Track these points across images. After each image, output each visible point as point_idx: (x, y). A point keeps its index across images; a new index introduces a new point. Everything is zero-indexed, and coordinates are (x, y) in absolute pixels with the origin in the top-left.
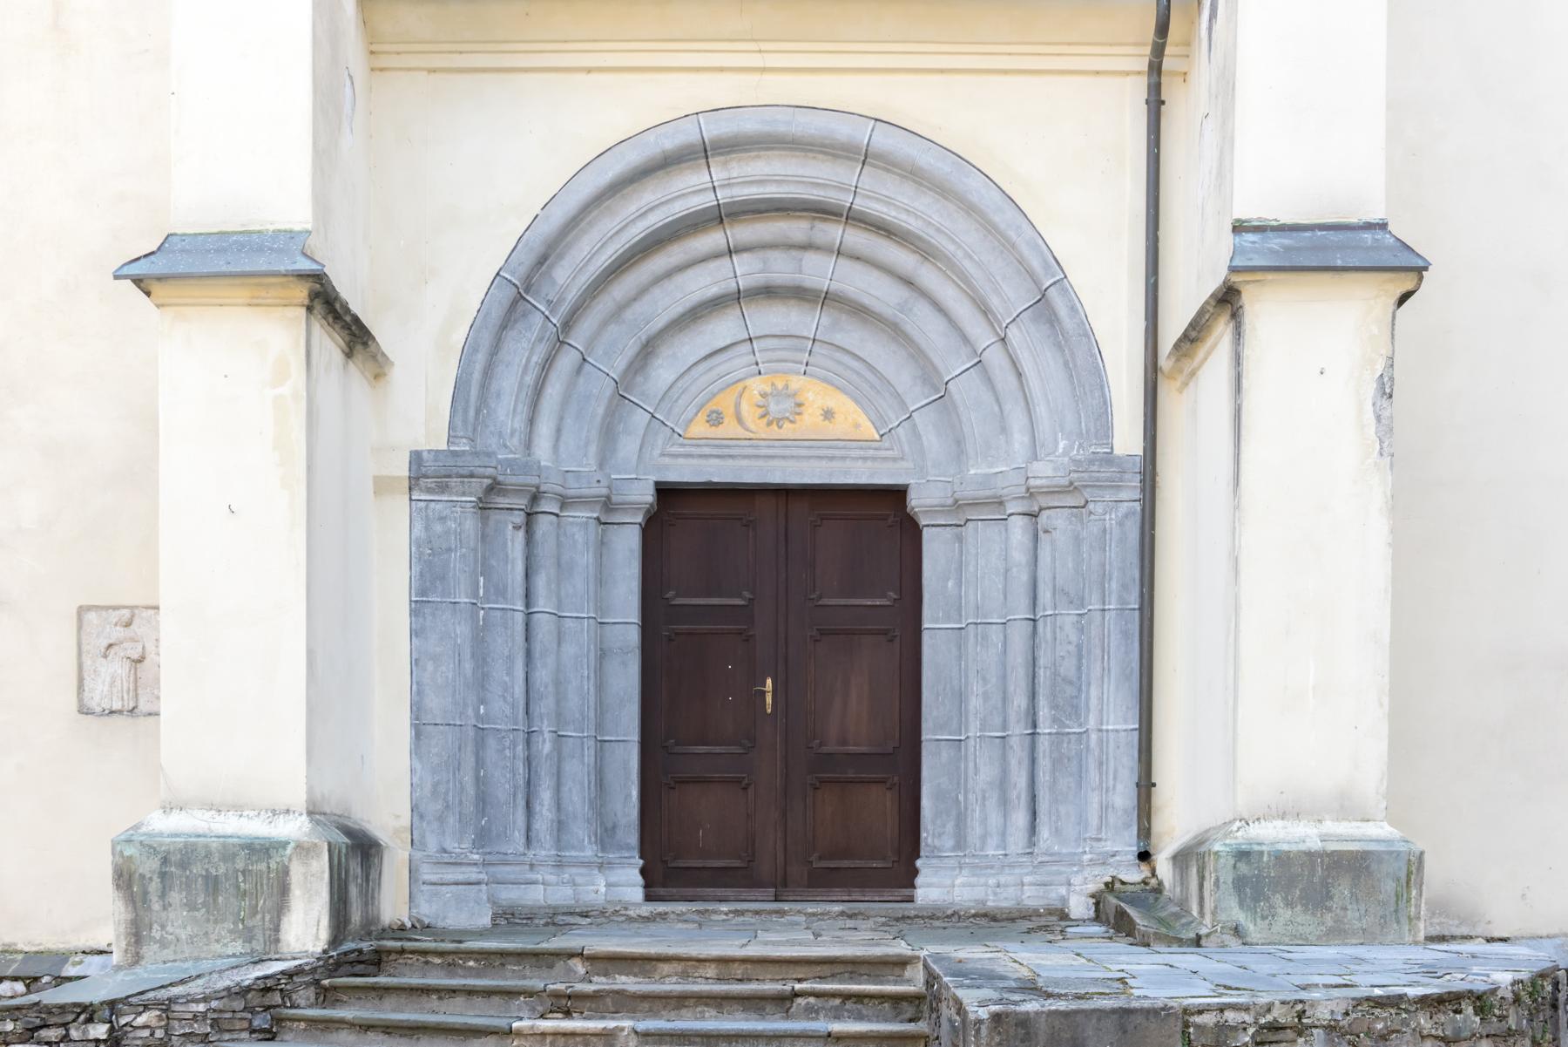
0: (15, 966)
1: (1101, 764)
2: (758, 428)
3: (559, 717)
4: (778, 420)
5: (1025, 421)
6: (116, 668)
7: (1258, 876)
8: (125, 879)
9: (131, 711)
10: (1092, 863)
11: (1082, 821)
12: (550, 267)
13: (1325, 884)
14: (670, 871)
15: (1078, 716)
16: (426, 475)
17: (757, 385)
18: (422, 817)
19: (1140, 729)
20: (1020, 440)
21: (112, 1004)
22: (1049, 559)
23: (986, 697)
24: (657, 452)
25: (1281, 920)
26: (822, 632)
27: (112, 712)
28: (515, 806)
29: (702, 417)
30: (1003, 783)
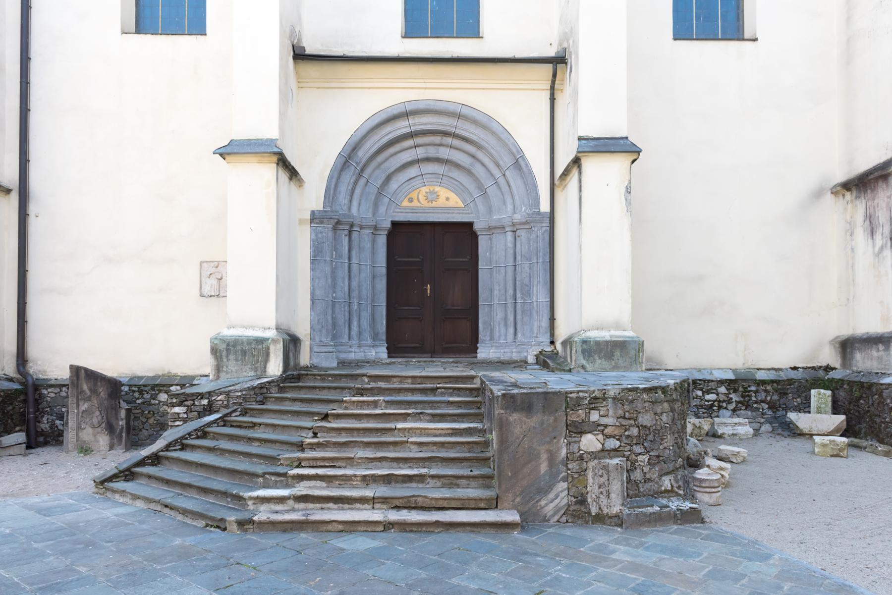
2: (425, 203)
3: (360, 298)
8: (214, 351)
11: (532, 331)
13: (611, 351)
14: (395, 349)
16: (316, 218)
17: (424, 190)
20: (510, 207)
21: (209, 393)
23: (500, 290)
29: (406, 199)
30: (506, 319)
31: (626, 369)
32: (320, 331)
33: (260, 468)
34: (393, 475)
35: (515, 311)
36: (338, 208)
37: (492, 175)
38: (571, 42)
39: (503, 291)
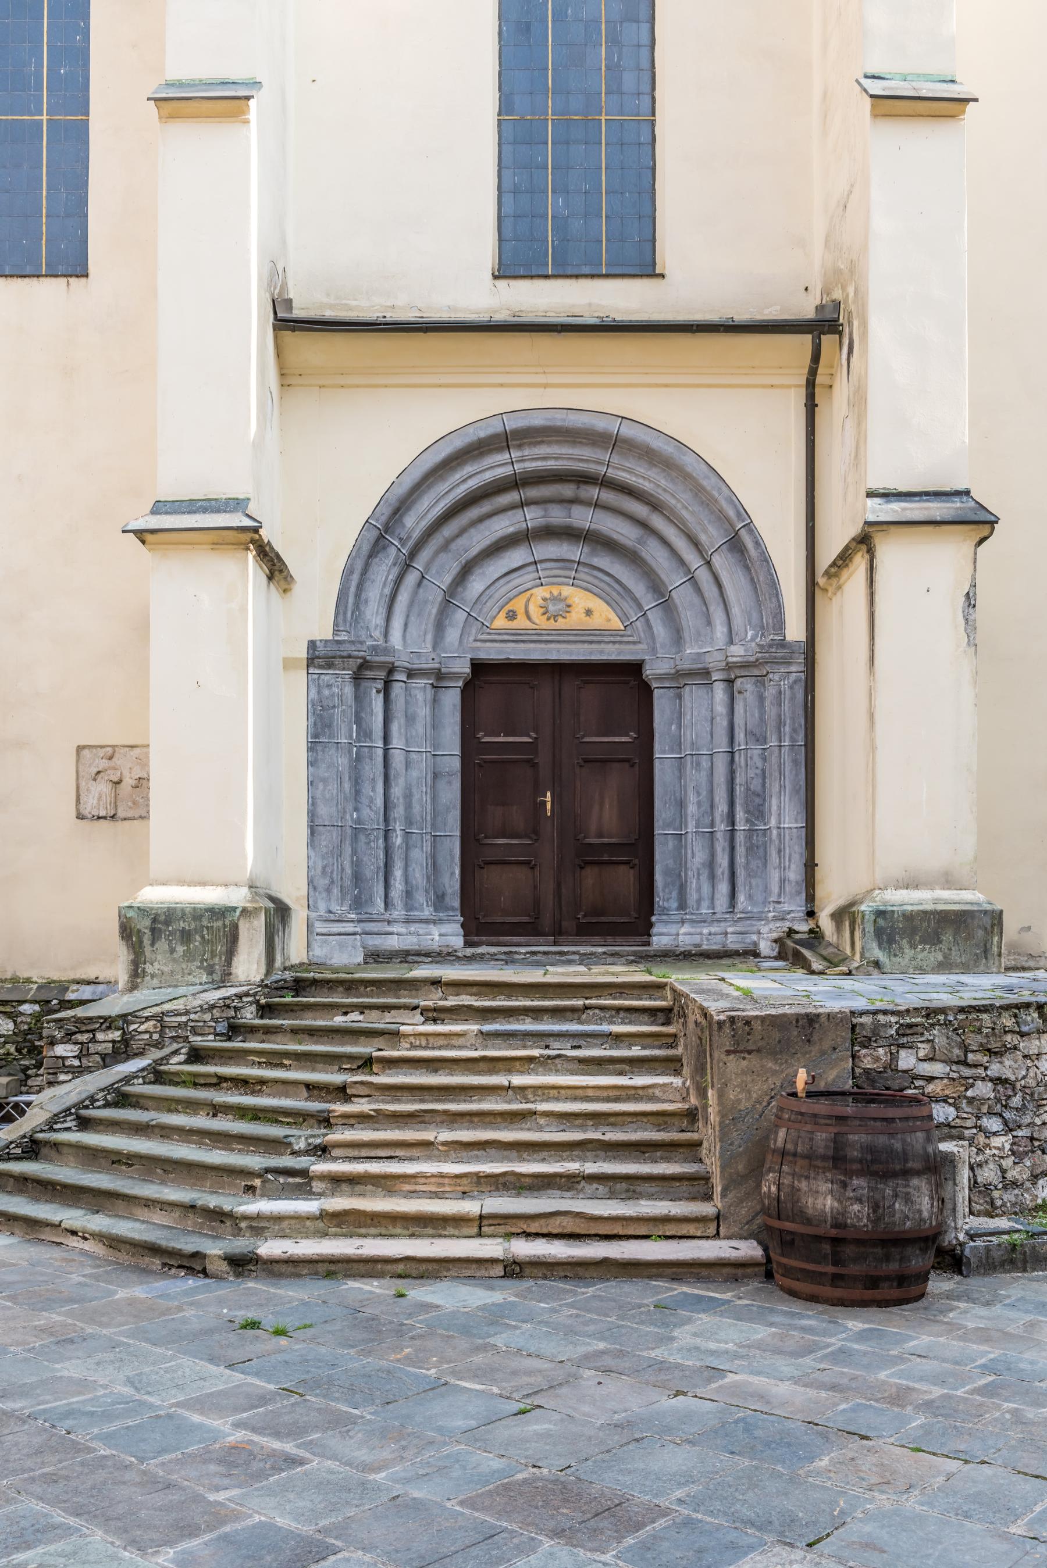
0: (32, 992)
1: (780, 851)
2: (541, 622)
3: (409, 821)
4: (555, 617)
5: (724, 617)
6: (103, 787)
7: (891, 927)
8: (127, 931)
9: (112, 817)
10: (776, 919)
11: (766, 889)
12: (401, 516)
14: (481, 924)
15: (763, 817)
16: (319, 658)
17: (540, 593)
18: (315, 888)
19: (806, 827)
20: (720, 630)
21: (124, 1017)
22: (742, 711)
23: (699, 804)
24: (472, 638)
25: (907, 957)
26: (586, 761)
27: (99, 818)
28: (378, 881)
29: (503, 614)
30: (711, 864)
31: (966, 968)
32: (328, 890)
33: (254, 1161)
34: (513, 1174)
35: (732, 849)
36: (363, 634)
37: (682, 562)
38: (851, 290)
39: (706, 806)
